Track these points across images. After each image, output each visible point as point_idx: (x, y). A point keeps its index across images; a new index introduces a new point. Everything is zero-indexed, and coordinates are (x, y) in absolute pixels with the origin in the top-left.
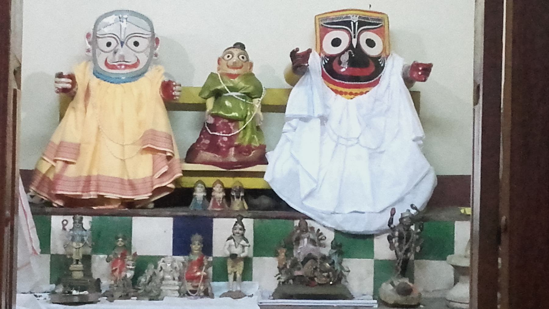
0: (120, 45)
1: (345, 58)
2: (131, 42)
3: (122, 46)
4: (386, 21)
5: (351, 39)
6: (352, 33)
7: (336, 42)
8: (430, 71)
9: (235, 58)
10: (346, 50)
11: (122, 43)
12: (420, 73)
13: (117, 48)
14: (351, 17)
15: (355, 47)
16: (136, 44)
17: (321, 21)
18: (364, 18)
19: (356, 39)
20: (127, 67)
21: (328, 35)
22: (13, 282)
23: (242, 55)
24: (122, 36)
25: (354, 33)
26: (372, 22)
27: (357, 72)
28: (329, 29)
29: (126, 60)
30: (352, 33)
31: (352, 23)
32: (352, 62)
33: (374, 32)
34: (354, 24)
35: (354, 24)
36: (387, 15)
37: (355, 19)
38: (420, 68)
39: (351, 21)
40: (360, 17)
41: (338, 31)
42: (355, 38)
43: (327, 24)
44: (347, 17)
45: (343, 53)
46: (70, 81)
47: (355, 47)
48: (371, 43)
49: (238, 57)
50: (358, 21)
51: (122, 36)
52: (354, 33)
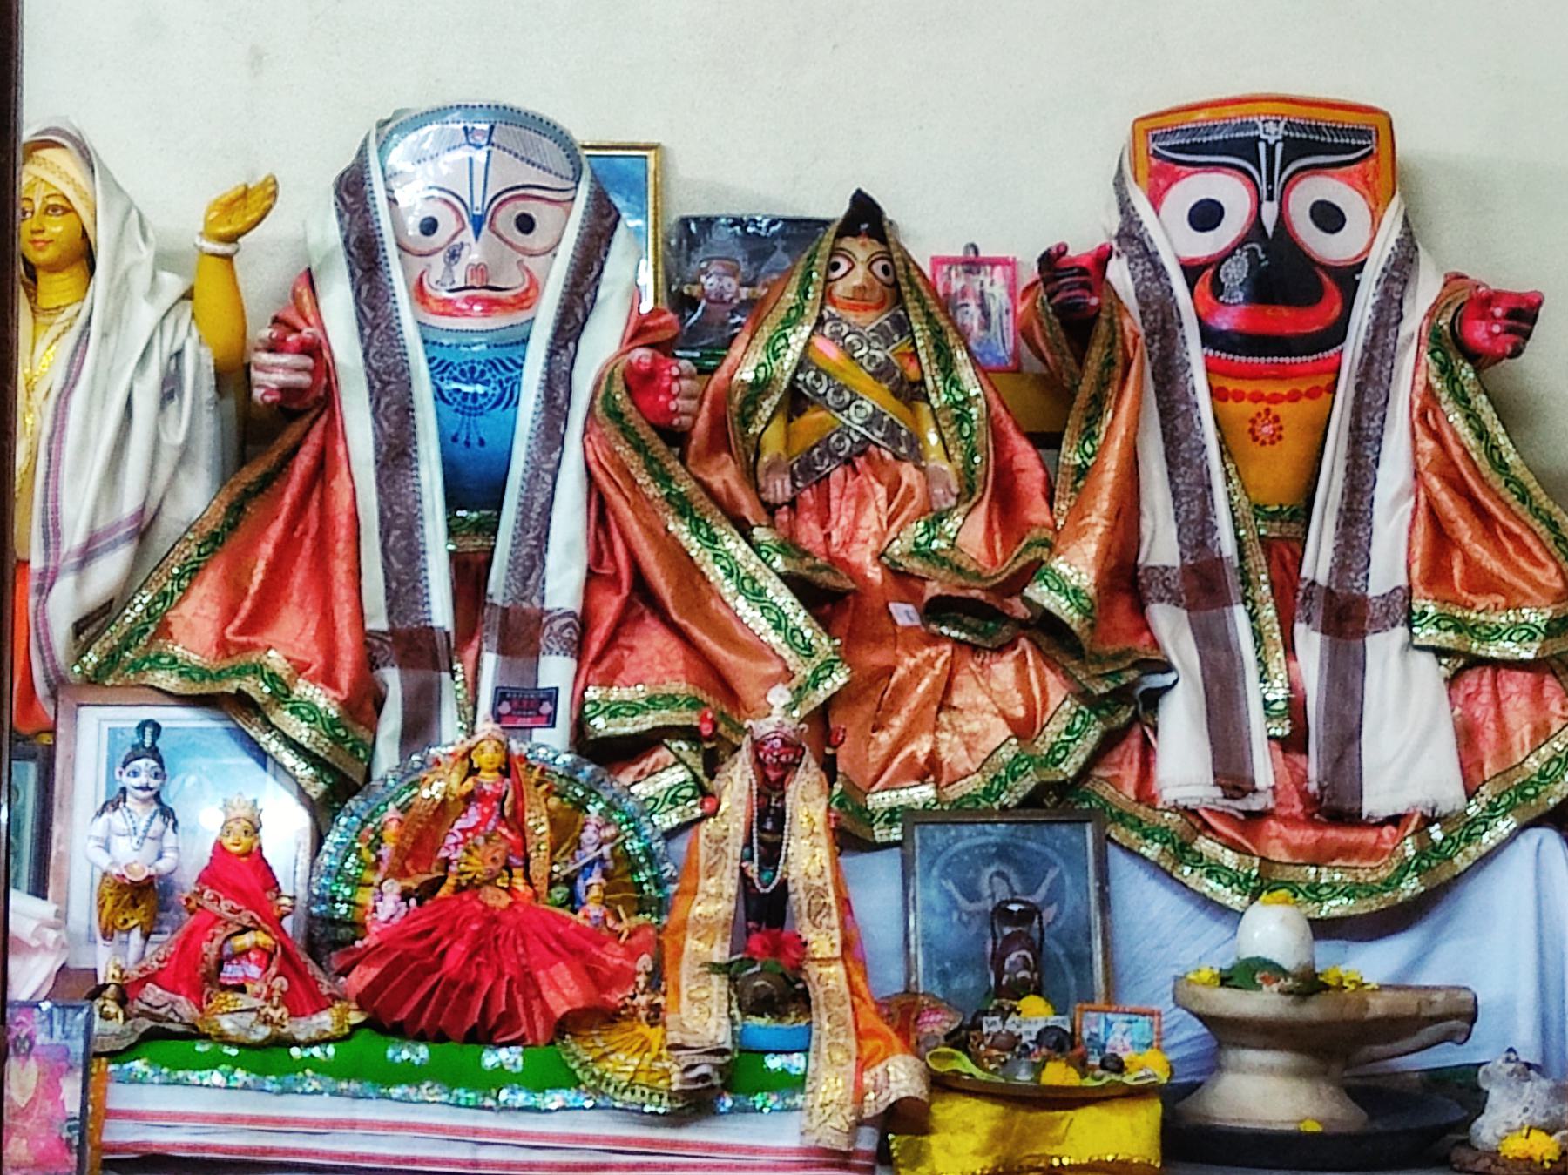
0: (470, 228)
1: (1236, 271)
2: (506, 219)
3: (477, 232)
4: (1384, 134)
5: (1259, 203)
6: (1263, 188)
7: (1206, 216)
8: (1533, 319)
9: (861, 270)
10: (1241, 243)
11: (478, 223)
12: (1496, 329)
13: (457, 241)
14: (1260, 125)
15: (1270, 230)
16: (526, 224)
17: (1155, 138)
18: (1302, 128)
19: (1275, 204)
20: (491, 306)
21: (1176, 189)
22: (1539, 1027)
23: (881, 263)
24: (478, 203)
25: (1270, 181)
26: (1340, 139)
27: (1282, 320)
28: (1179, 168)
29: (491, 283)
30: (1263, 188)
31: (1262, 146)
32: (1262, 289)
33: (1341, 177)
34: (1271, 150)
35: (1271, 150)
36: (1386, 114)
37: (1272, 133)
38: (1498, 312)
39: (1258, 139)
40: (1290, 126)
41: (1215, 176)
42: (1270, 198)
43: (1178, 145)
44: (1245, 126)
45: (1229, 253)
46: (309, 362)
47: (1270, 230)
48: (1329, 217)
49: (870, 267)
50: (1285, 139)
51: (478, 203)
52: (1270, 181)
